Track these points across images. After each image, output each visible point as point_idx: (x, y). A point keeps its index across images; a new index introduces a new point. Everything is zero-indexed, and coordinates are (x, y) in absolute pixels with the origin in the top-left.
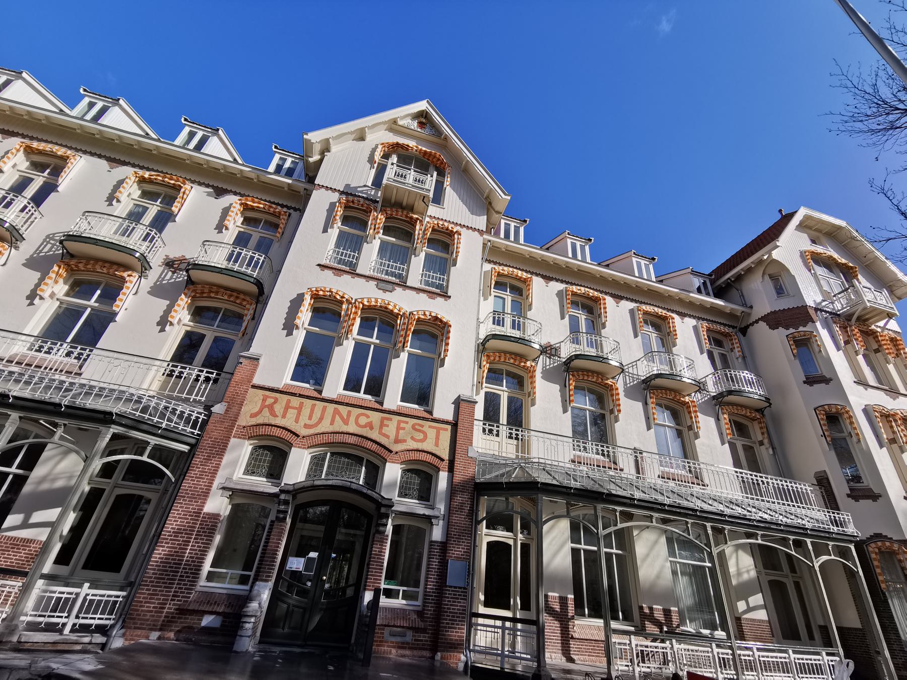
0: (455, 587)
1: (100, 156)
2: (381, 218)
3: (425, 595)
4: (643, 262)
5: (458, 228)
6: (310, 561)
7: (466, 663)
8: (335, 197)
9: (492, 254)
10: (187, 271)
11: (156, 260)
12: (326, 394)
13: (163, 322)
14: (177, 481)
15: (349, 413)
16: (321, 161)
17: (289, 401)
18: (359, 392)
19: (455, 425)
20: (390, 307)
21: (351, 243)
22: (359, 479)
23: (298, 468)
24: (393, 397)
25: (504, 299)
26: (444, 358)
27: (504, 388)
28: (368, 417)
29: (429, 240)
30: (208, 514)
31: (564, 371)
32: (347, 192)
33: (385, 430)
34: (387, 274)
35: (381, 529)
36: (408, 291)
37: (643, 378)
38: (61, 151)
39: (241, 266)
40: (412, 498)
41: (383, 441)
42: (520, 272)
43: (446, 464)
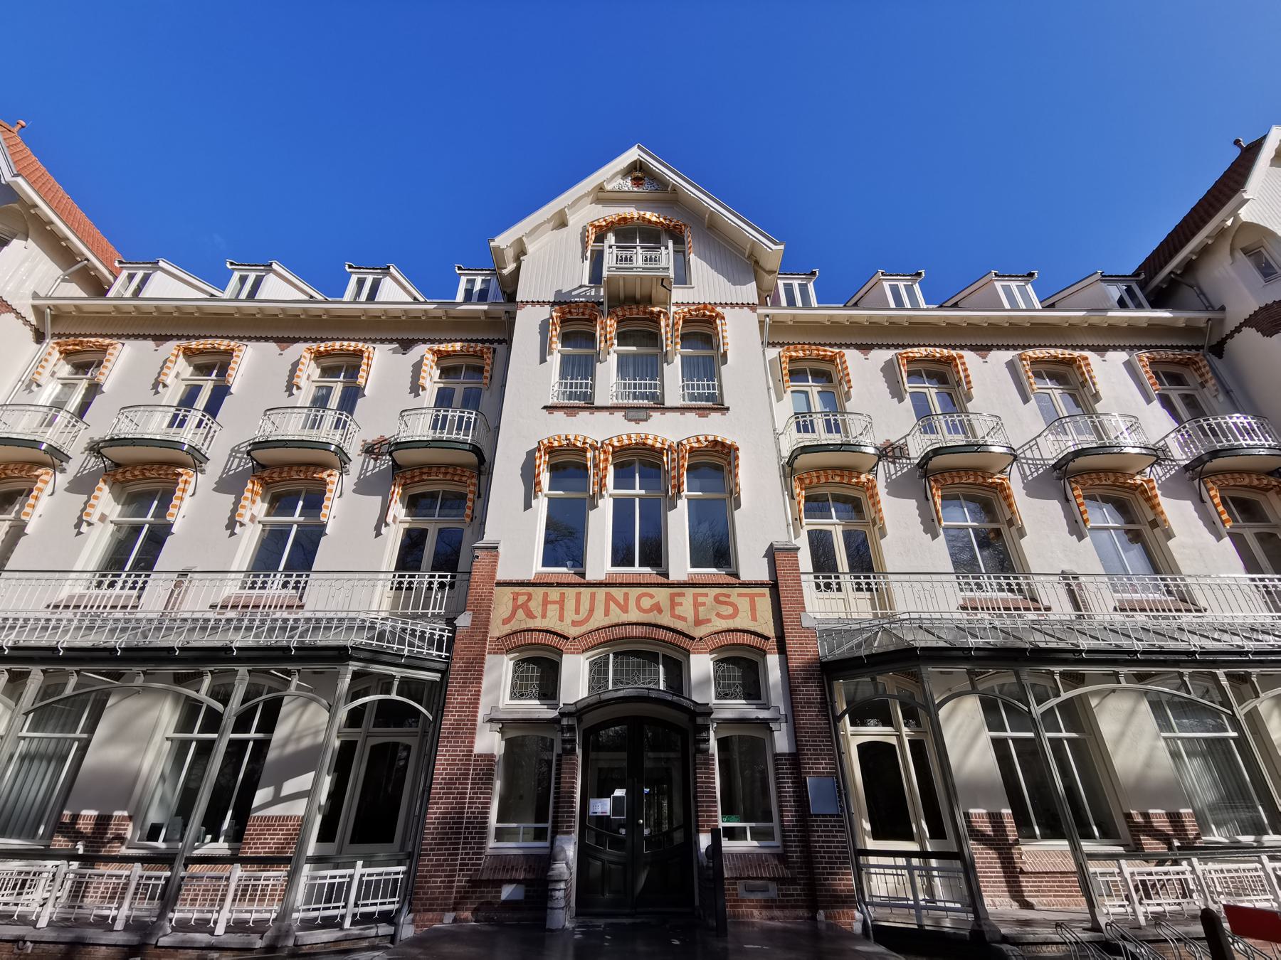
0: (824, 816)
2: (611, 324)
4: (1014, 285)
7: (865, 923)
9: (774, 333)
11: (354, 450)
13: (382, 521)
14: (435, 718)
16: (518, 269)
17: (546, 595)
18: (633, 565)
19: (774, 587)
20: (650, 442)
21: (580, 369)
24: (680, 563)
25: (806, 393)
27: (835, 520)
28: (652, 596)
31: (921, 477)
33: (678, 610)
34: (635, 397)
35: (703, 746)
38: (223, 344)
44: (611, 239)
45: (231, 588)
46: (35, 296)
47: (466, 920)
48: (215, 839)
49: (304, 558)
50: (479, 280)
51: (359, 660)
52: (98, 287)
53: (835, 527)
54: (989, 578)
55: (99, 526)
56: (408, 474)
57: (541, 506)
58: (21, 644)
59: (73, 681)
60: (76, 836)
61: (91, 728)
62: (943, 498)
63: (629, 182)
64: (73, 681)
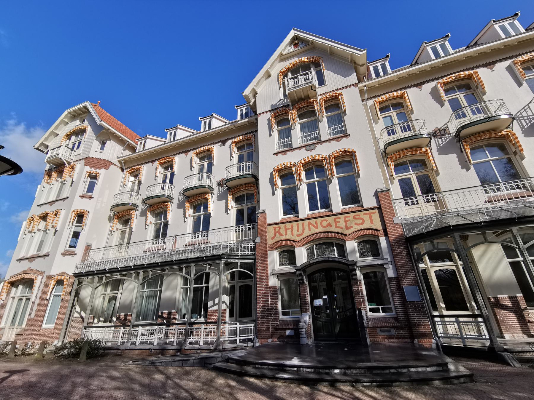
0: (413, 302)
1: (181, 153)
2: (294, 112)
3: (396, 309)
4: (506, 24)
5: (340, 91)
6: (324, 300)
7: (437, 344)
8: (268, 115)
9: (366, 94)
10: (225, 184)
11: (214, 186)
12: (301, 217)
13: (227, 209)
14: (254, 275)
15: (316, 222)
16: (256, 100)
17: (285, 226)
18: (318, 209)
19: (379, 208)
20: (317, 158)
21: (285, 134)
22: (334, 254)
23: (302, 256)
24: (337, 205)
25: (390, 116)
26: (358, 172)
27: (412, 172)
28: (327, 221)
29: (326, 109)
30: (271, 287)
31: (457, 142)
32: (273, 109)
33: (338, 225)
34: (310, 140)
35: (354, 277)
36: (324, 144)
37: (454, 134)
38: (206, 148)
39: (243, 172)
40: (368, 257)
41: (339, 230)
42: (395, 93)
43: (382, 232)
44: (290, 75)
45: (188, 239)
46: (118, 158)
47: (276, 341)
48: (200, 318)
49: (206, 227)
50: (244, 109)
51: (224, 258)
52: (133, 149)
53: (412, 176)
54: (504, 184)
55: (150, 225)
56: (233, 190)
57: (279, 193)
58: (136, 264)
59: (151, 273)
60: (163, 319)
61: (161, 287)
62: (471, 149)
63: (292, 47)
64: (151, 273)
